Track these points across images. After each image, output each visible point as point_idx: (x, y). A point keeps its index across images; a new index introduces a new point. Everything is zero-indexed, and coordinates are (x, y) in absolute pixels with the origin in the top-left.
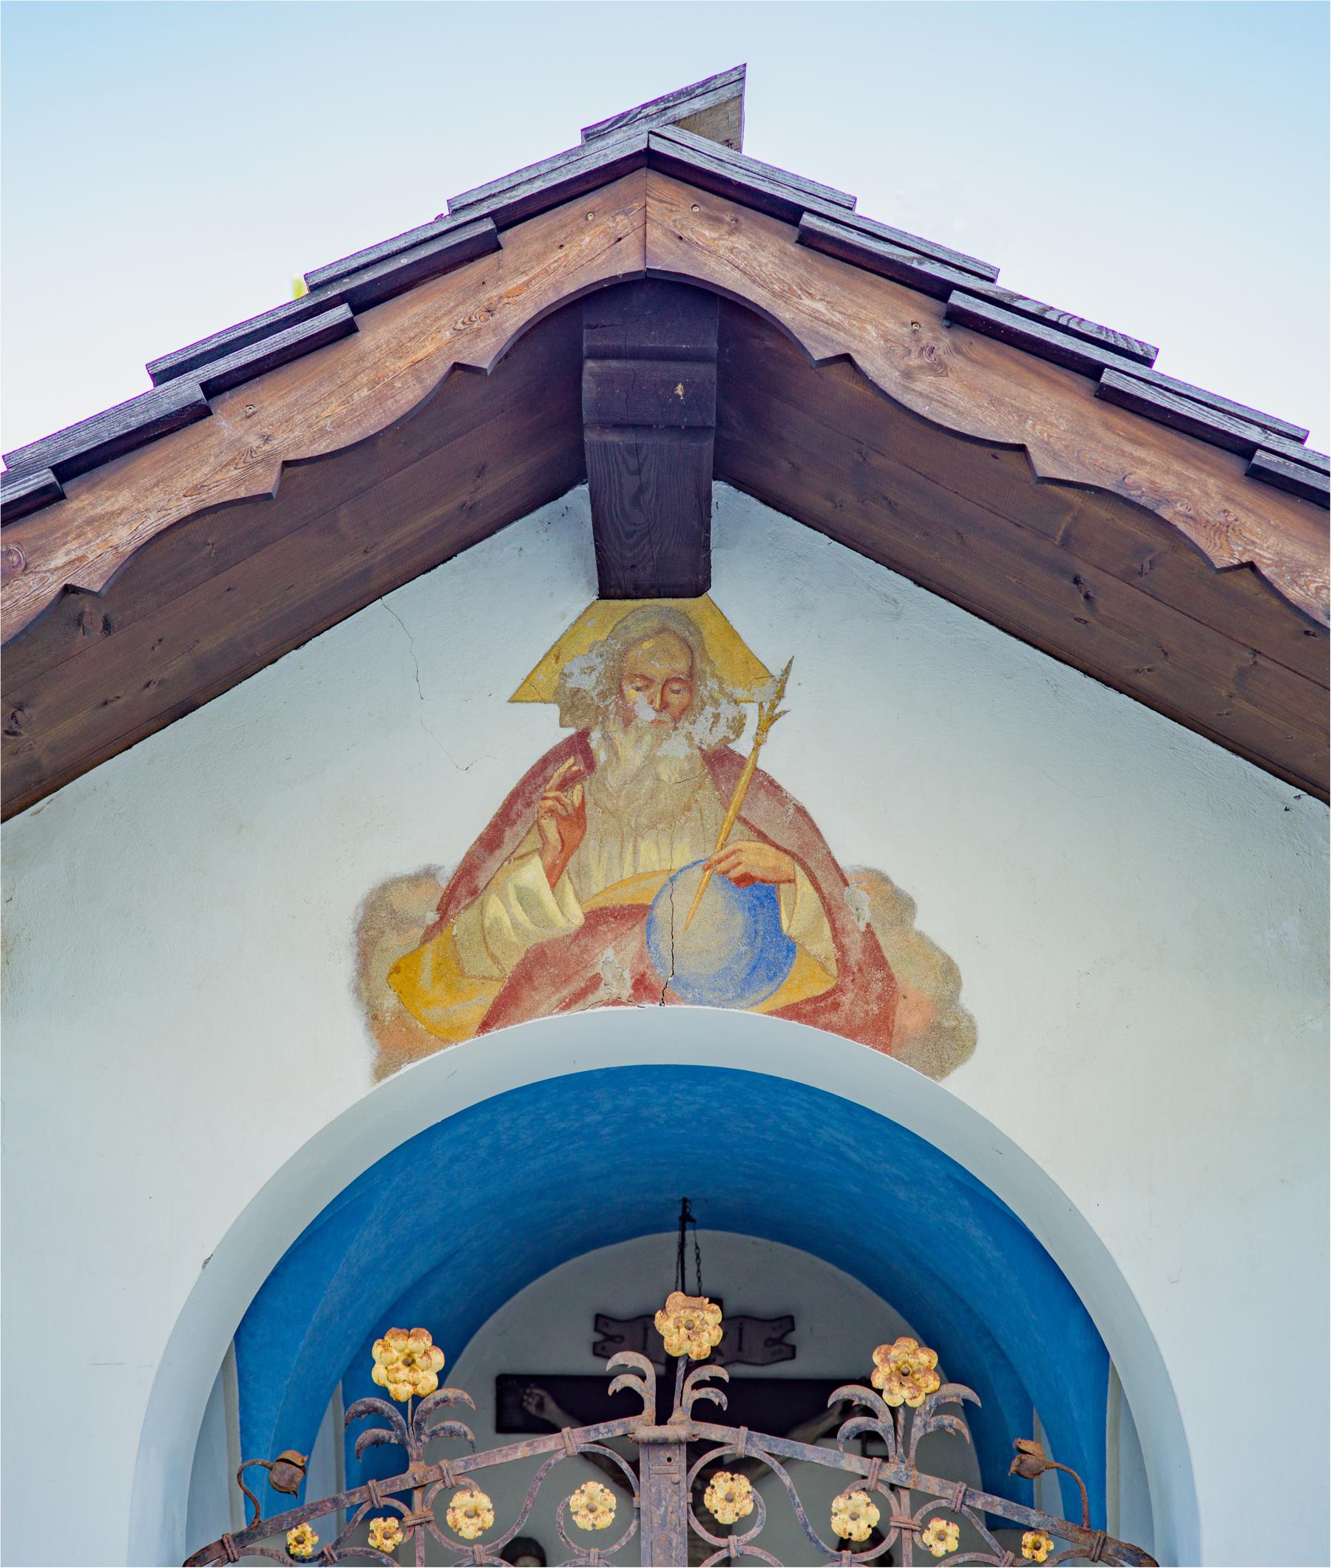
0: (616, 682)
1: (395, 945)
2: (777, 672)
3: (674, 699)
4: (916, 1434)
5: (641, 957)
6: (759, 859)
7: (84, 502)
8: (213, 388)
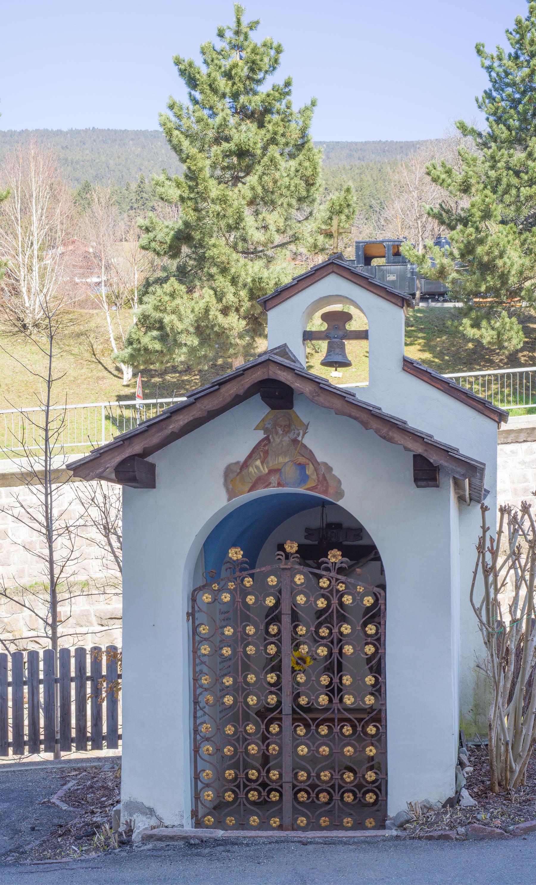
0: (275, 425)
1: (232, 476)
2: (306, 424)
3: (286, 429)
4: (337, 567)
5: (279, 479)
6: (302, 460)
7: (175, 418)
8: (195, 399)
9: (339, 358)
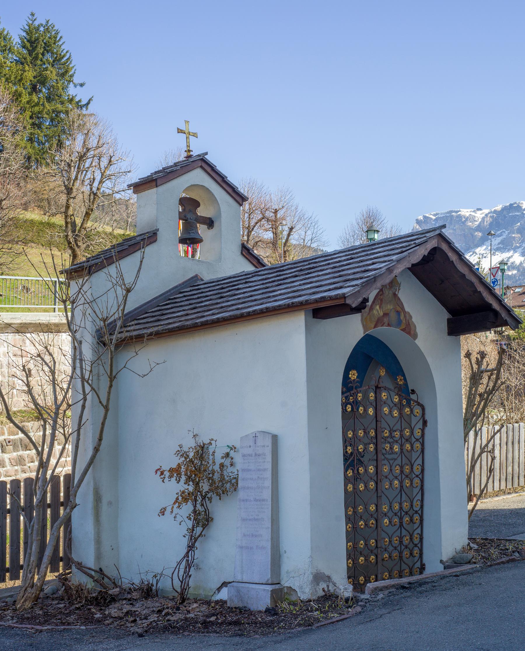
6: (398, 309)
9: (192, 236)
